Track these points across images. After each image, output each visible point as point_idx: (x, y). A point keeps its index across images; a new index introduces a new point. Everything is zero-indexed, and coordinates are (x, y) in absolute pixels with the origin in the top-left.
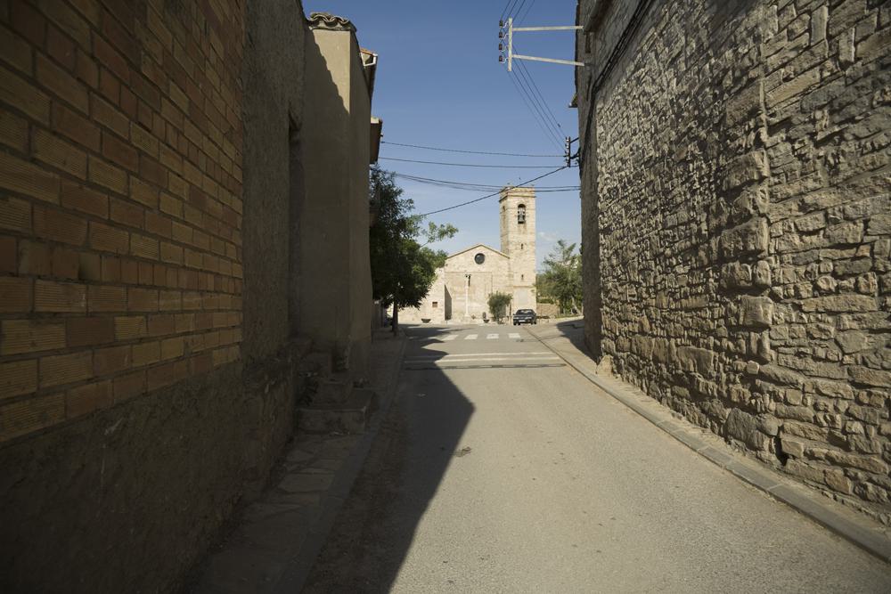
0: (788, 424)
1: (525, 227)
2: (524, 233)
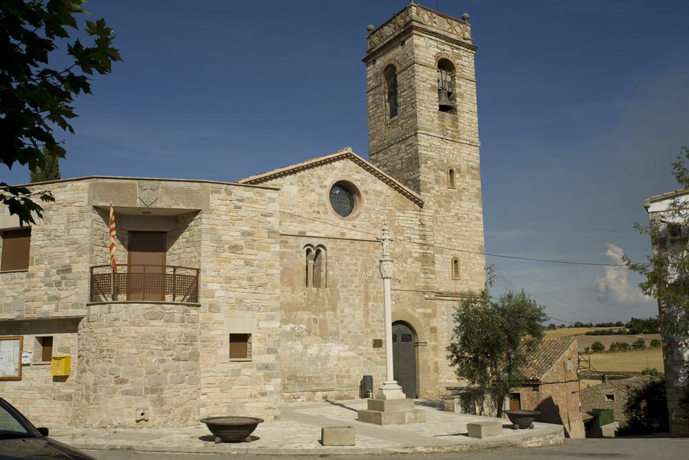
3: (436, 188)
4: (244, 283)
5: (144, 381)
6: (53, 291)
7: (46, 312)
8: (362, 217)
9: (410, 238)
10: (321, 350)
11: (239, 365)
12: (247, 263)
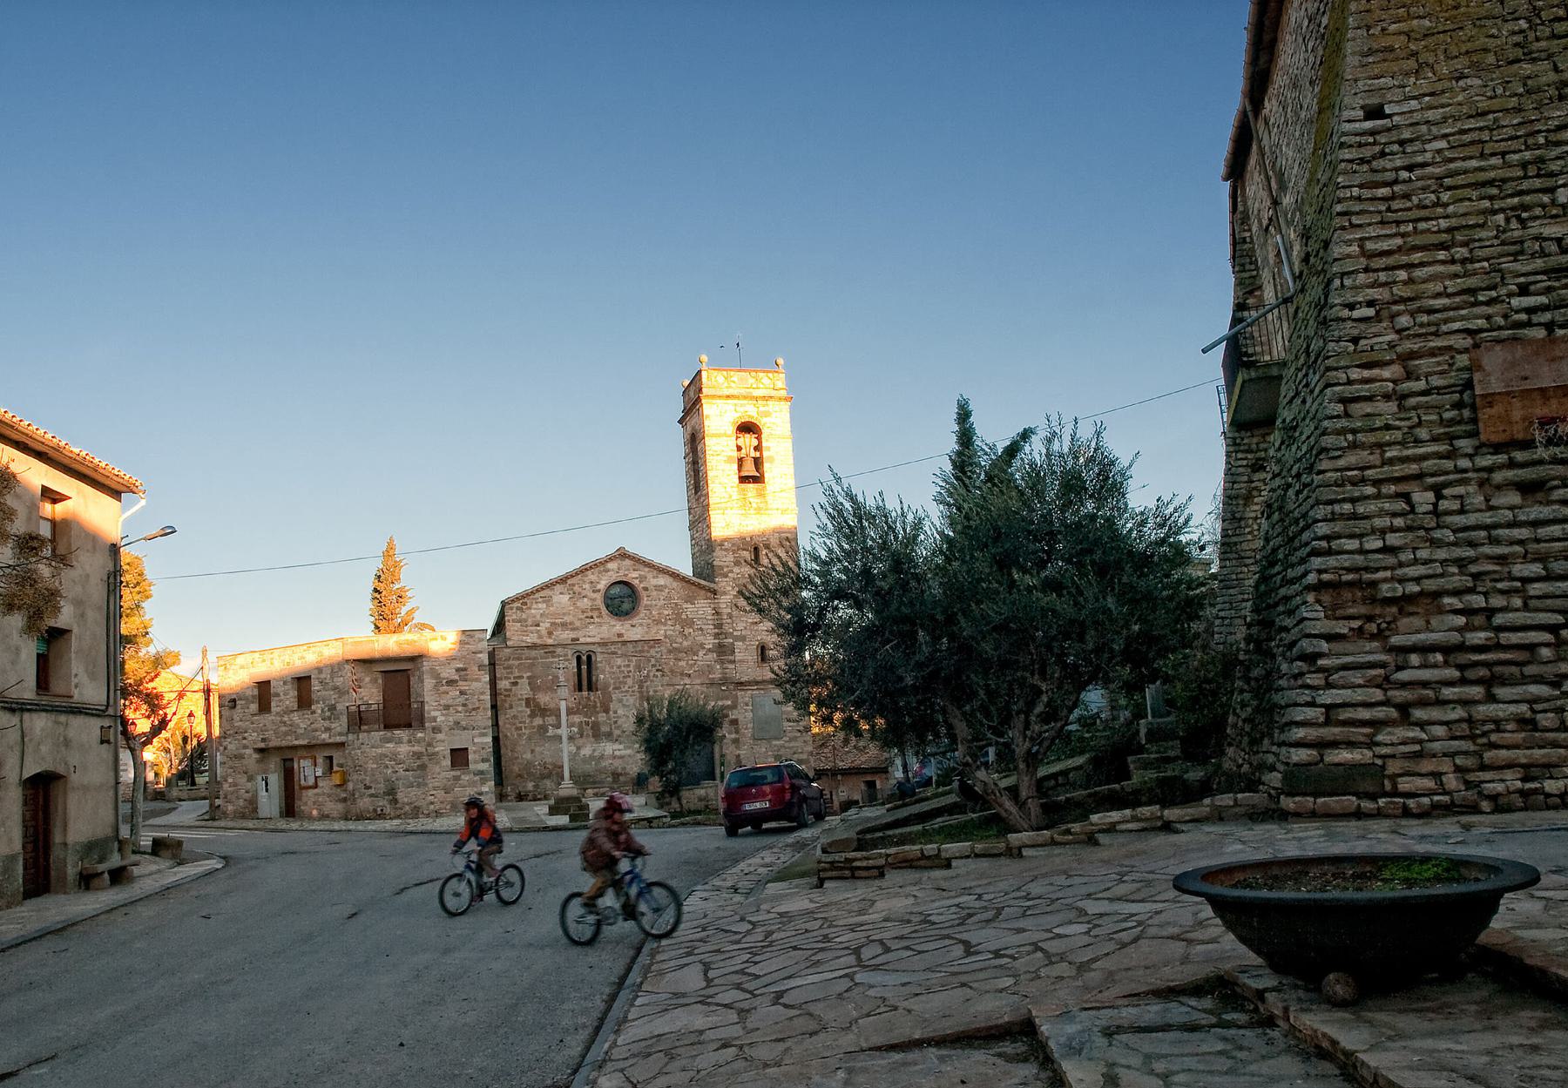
0: (1202, 774)
1: (761, 495)
2: (759, 510)
3: (736, 570)
4: (460, 709)
5: (382, 787)
6: (327, 724)
7: (324, 739)
8: (642, 615)
9: (701, 629)
10: (594, 750)
11: (458, 773)
12: (462, 693)
